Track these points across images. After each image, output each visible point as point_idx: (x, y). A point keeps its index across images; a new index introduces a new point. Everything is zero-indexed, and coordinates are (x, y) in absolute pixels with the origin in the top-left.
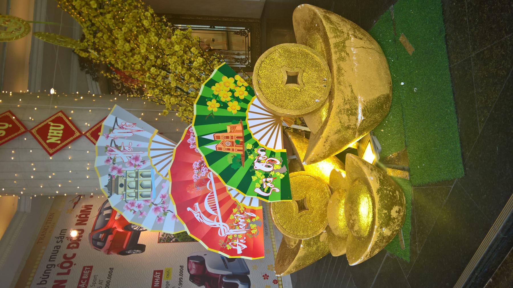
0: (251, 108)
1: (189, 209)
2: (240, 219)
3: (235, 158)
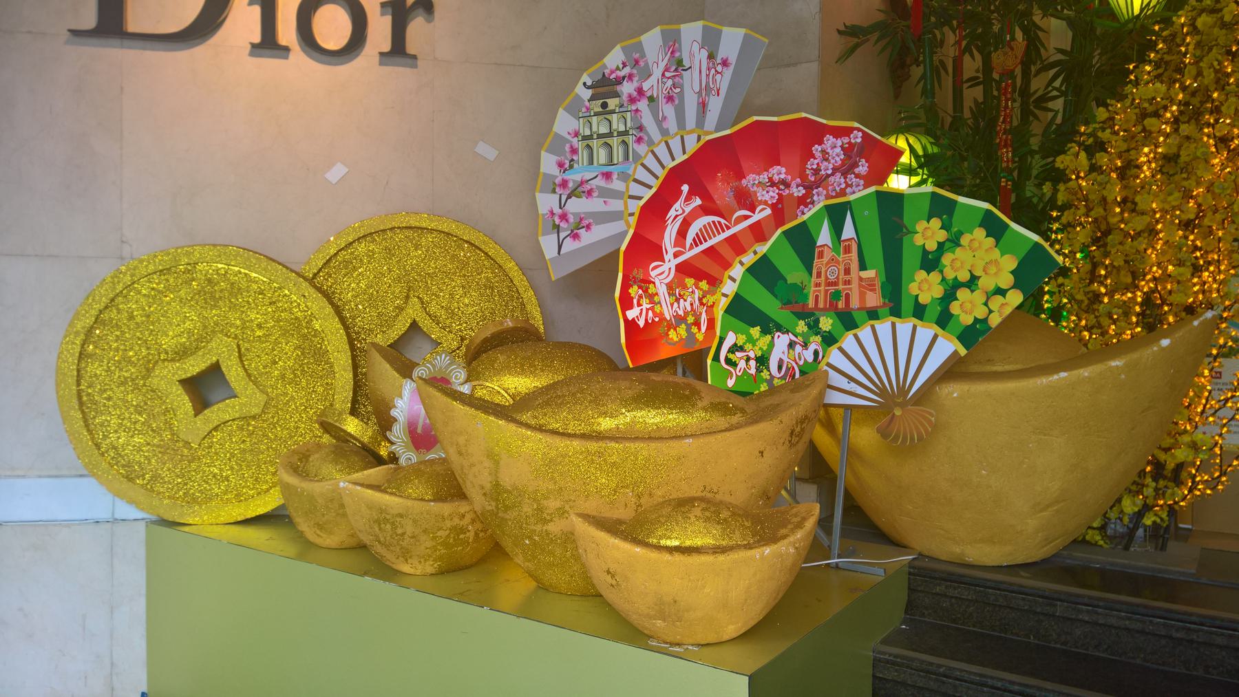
0: (926, 332)
1: (685, 188)
2: (689, 300)
3: (800, 289)
